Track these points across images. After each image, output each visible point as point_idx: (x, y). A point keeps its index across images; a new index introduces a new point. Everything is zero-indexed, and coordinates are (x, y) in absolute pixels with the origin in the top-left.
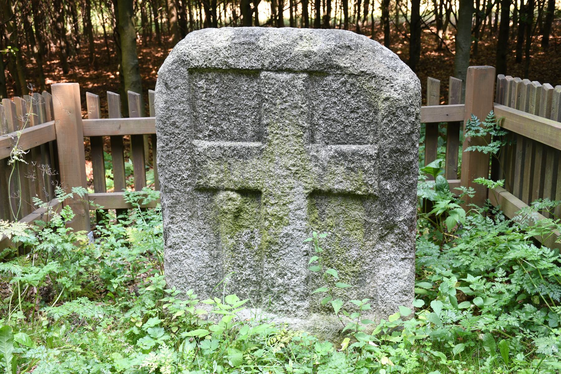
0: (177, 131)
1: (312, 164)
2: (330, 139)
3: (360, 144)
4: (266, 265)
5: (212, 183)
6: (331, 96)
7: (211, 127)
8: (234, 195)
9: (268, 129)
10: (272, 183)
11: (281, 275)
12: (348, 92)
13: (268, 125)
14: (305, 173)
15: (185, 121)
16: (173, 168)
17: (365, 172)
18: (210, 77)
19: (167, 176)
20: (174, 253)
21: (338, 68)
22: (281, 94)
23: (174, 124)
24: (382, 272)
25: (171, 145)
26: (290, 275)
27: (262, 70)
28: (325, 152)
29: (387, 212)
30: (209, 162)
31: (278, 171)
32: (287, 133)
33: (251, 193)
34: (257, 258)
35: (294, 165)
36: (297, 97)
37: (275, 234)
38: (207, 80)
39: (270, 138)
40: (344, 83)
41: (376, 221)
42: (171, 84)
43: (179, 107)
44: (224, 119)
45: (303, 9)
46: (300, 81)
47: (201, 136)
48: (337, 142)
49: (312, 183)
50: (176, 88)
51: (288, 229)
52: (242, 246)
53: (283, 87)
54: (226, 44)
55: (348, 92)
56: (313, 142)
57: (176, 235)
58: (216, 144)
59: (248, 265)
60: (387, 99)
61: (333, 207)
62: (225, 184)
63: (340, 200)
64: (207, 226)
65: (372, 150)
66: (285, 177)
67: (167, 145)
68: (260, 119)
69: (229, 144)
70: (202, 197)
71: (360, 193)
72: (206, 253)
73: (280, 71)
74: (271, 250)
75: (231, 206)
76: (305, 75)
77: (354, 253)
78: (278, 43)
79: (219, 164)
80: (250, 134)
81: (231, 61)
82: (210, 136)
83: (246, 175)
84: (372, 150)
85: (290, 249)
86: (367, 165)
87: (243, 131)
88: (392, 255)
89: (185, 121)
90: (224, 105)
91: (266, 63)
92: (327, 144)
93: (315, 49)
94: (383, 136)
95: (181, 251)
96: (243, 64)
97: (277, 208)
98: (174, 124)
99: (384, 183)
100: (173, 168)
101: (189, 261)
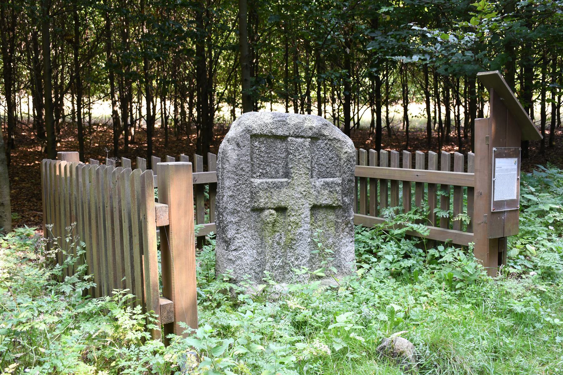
0: (244, 173)
1: (313, 190)
2: (321, 175)
3: (333, 177)
4: (289, 254)
5: (262, 205)
6: (320, 151)
7: (261, 171)
8: (273, 212)
9: (292, 170)
10: (293, 202)
11: (297, 259)
12: (328, 149)
13: (292, 168)
14: (309, 195)
15: (248, 167)
16: (240, 197)
17: (337, 193)
18: (261, 140)
19: (236, 203)
20: (238, 253)
21: (324, 136)
22: (298, 150)
23: (242, 169)
24: (343, 250)
25: (240, 182)
26: (301, 258)
27: (289, 136)
28: (319, 182)
29: (346, 215)
30: (261, 191)
31: (297, 195)
32: (301, 172)
33: (281, 210)
34: (283, 250)
35: (304, 191)
36: (306, 152)
37: (294, 234)
38: (259, 142)
39: (293, 175)
40: (326, 144)
41: (340, 221)
42: (241, 144)
43: (246, 158)
44: (268, 165)
45: (381, 123)
46: (307, 142)
47: (255, 176)
48: (323, 177)
49: (313, 201)
50: (244, 146)
51: (300, 230)
52: (275, 244)
53: (300, 146)
54: (271, 121)
55: (328, 149)
56: (312, 177)
57: (239, 241)
58: (264, 180)
59: (278, 255)
60: (346, 152)
61: (321, 214)
62: (269, 205)
63: (324, 210)
64: (256, 233)
65: (338, 180)
66: (300, 198)
67: (238, 182)
68: (287, 165)
69: (270, 180)
70: (254, 215)
71: (334, 205)
72: (255, 251)
73: (297, 137)
74: (290, 245)
75: (271, 219)
76: (310, 139)
77: (331, 240)
78: (296, 122)
79: (266, 193)
80: (281, 173)
81: (273, 131)
82: (260, 176)
83: (280, 199)
84: (338, 180)
85: (301, 242)
86: (338, 189)
87: (277, 172)
88: (347, 240)
89: (248, 167)
90: (268, 157)
91: (291, 133)
92: (318, 178)
93: (314, 125)
94: (344, 172)
95: (242, 251)
96: (280, 133)
97: (296, 218)
98: (242, 169)
99: (345, 198)
100: (240, 197)
101: (246, 258)
